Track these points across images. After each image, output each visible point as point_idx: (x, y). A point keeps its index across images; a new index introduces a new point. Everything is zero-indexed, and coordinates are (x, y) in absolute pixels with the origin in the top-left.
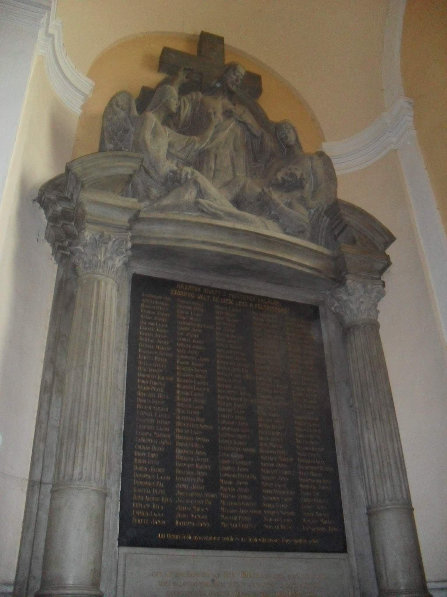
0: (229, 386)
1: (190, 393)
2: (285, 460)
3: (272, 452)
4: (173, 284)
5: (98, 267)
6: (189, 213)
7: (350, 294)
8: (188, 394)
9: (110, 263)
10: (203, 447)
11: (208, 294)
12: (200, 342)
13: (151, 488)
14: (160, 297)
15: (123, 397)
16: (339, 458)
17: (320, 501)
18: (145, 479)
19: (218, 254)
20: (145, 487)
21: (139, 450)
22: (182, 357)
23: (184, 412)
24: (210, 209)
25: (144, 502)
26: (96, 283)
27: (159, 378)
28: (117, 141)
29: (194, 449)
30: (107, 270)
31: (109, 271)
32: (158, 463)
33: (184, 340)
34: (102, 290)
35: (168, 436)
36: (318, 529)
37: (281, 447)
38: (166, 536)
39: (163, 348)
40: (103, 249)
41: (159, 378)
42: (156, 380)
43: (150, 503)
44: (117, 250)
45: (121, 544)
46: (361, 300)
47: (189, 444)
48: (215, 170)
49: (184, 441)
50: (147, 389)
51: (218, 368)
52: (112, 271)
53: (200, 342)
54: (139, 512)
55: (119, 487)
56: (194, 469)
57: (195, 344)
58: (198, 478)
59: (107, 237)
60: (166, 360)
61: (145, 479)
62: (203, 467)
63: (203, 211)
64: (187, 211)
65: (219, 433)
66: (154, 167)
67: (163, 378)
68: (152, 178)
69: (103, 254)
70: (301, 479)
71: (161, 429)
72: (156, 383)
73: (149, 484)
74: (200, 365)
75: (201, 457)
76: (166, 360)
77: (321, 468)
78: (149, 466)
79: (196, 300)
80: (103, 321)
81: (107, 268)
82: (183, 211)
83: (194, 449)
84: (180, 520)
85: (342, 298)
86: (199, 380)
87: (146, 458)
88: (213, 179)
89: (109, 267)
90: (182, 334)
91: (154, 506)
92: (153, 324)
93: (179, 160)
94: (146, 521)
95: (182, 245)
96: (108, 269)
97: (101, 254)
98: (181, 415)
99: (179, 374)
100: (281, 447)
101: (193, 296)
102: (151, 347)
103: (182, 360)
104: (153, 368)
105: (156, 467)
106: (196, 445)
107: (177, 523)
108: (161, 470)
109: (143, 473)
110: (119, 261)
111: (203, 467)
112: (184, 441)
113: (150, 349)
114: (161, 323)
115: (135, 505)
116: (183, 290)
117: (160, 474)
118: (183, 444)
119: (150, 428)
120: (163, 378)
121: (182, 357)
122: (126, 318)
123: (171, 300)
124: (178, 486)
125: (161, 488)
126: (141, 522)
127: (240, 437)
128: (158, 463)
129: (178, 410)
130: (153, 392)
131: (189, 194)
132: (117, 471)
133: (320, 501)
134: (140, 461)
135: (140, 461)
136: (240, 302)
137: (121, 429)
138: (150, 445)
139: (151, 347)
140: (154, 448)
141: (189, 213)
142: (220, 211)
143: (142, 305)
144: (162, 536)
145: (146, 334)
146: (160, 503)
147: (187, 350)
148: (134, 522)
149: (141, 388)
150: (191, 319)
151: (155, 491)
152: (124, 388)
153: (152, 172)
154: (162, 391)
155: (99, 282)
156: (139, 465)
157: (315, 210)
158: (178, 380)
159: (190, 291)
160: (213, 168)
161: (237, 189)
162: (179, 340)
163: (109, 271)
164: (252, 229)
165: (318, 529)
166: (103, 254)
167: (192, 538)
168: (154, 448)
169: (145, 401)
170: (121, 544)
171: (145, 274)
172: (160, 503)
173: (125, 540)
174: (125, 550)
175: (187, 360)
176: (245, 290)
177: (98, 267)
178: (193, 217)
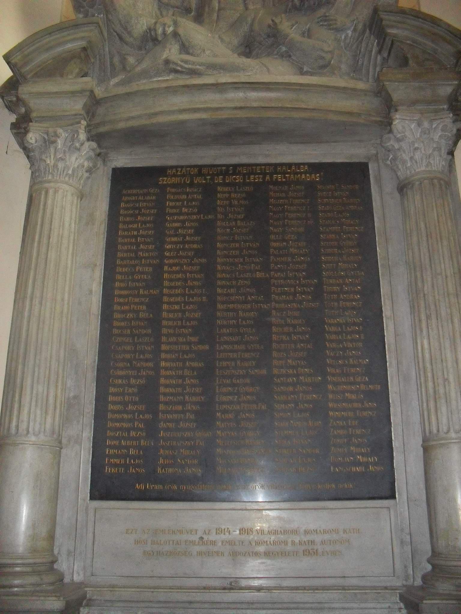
0: (232, 291)
1: (181, 307)
2: (309, 380)
3: (290, 371)
4: (162, 171)
5: (47, 173)
6: (160, 79)
7: (398, 140)
8: (177, 307)
9: (60, 165)
10: (195, 373)
11: (208, 174)
12: (196, 239)
13: (128, 430)
14: (145, 191)
15: (98, 322)
16: (391, 371)
17: (358, 432)
18: (122, 420)
19: (203, 122)
20: (121, 429)
21: (114, 386)
22: (171, 261)
23: (171, 331)
24: (186, 66)
25: (119, 447)
26: (43, 193)
27: (141, 292)
28: (88, 8)
29: (183, 377)
30: (57, 175)
31: (60, 175)
32: (137, 399)
33: (174, 239)
34: (49, 202)
35: (151, 364)
36: (354, 469)
37: (304, 363)
38: (145, 487)
39: (147, 255)
40: (52, 150)
41: (141, 292)
42: (138, 296)
43: (127, 448)
44: (70, 146)
45: (93, 497)
46: (416, 145)
47: (177, 371)
48: (219, 10)
49: (171, 369)
50: (126, 308)
51: (219, 267)
52: (65, 173)
53: (196, 239)
54: (113, 460)
55: (90, 432)
56: (183, 403)
57: (189, 242)
58: (187, 414)
59: (53, 134)
60: (151, 269)
61: (122, 420)
62: (194, 399)
63: (176, 71)
64: (156, 77)
65: (217, 353)
66: (126, 29)
67: (146, 292)
68: (127, 44)
69: (52, 157)
70: (330, 405)
71: (142, 357)
72: (137, 300)
73: (125, 425)
74: (194, 268)
75: (193, 386)
76: (151, 269)
77: (363, 387)
78: (125, 404)
79: (192, 185)
80: (49, 238)
81: (58, 173)
82: (151, 77)
83: (183, 377)
84: (164, 467)
85: (393, 146)
86: (192, 288)
87: (123, 394)
88: (217, 22)
89: (59, 170)
90: (172, 232)
91: (132, 452)
92: (135, 226)
93: (175, 9)
94: (121, 470)
95: (154, 120)
96: (59, 172)
97: (50, 156)
98: (168, 335)
99: (166, 283)
100: (304, 363)
101: (188, 181)
102: (133, 255)
103: (171, 265)
104: (134, 280)
105: (135, 403)
106: (187, 372)
107: (159, 470)
108: (142, 407)
109: (119, 412)
110: (77, 159)
111: (194, 399)
112: (171, 369)
113: (131, 259)
114: (145, 223)
115: (109, 452)
116: (175, 175)
117: (140, 412)
118: (169, 373)
119: (128, 356)
120: (146, 292)
121: (171, 261)
122: (104, 224)
123: (159, 191)
124: (162, 425)
125: (141, 430)
126: (115, 471)
127: (247, 355)
128: (137, 399)
129: (164, 331)
130: (134, 311)
131: (168, 52)
132: (89, 412)
133: (358, 432)
134: (116, 399)
135: (116, 399)
136: (252, 177)
137: (94, 362)
138: (127, 377)
139: (133, 255)
140: (133, 381)
141: (160, 79)
142: (200, 66)
143: (123, 205)
144: (141, 487)
145: (126, 240)
146: (139, 447)
147: (178, 251)
148: (108, 470)
149: (119, 308)
150: (184, 210)
151: (133, 434)
152: (99, 311)
153: (125, 36)
154: (144, 308)
155: (47, 192)
156: (114, 403)
157: (352, 30)
158: (165, 291)
159: (183, 176)
160: (217, 8)
161: (245, 28)
162: (168, 240)
163: (60, 175)
164: (243, 78)
165: (354, 469)
166: (52, 157)
167: (178, 488)
168: (133, 381)
169: (123, 324)
170: (93, 497)
171: (129, 166)
172: (139, 447)
173: (97, 493)
174: (97, 504)
175: (175, 265)
176: (261, 160)
177: (47, 173)
178: (171, 80)
